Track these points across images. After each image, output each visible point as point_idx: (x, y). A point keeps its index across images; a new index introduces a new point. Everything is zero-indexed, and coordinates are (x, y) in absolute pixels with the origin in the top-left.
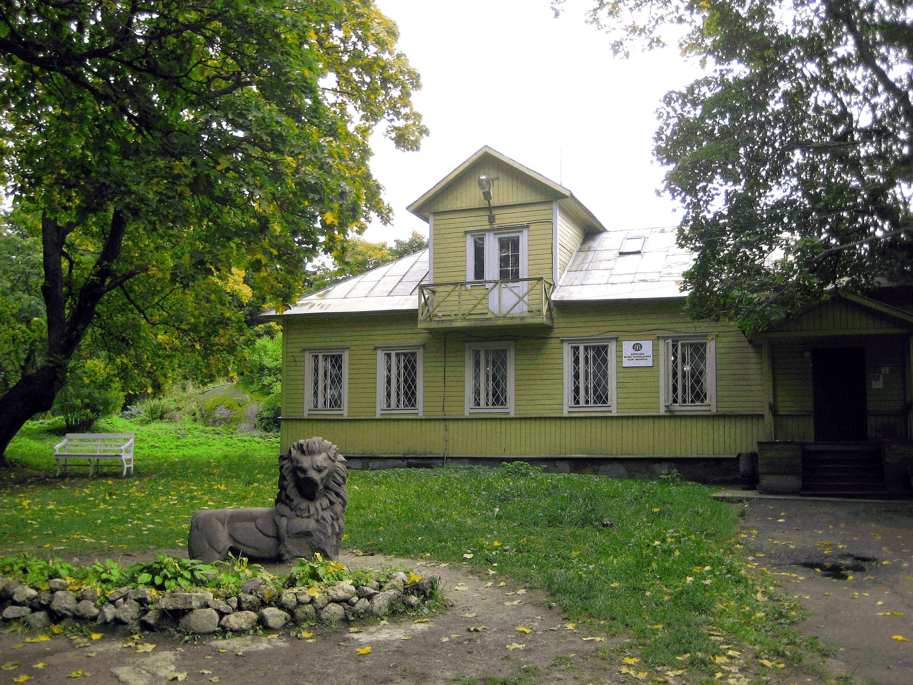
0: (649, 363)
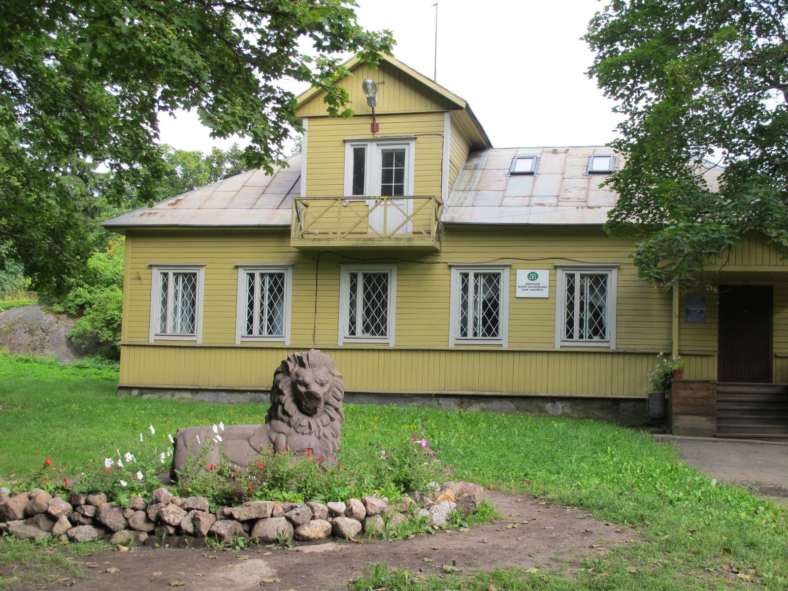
0: (545, 293)
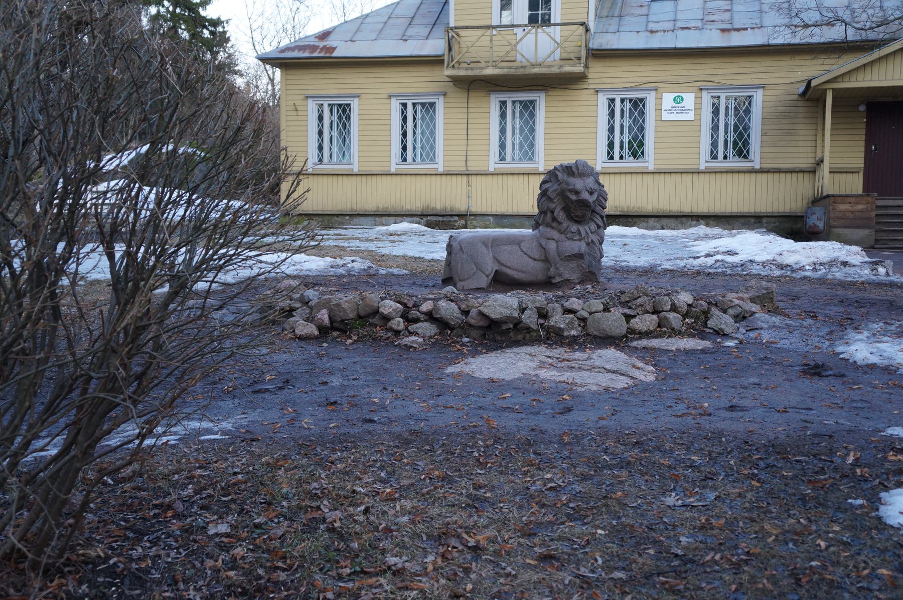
0: (690, 116)
